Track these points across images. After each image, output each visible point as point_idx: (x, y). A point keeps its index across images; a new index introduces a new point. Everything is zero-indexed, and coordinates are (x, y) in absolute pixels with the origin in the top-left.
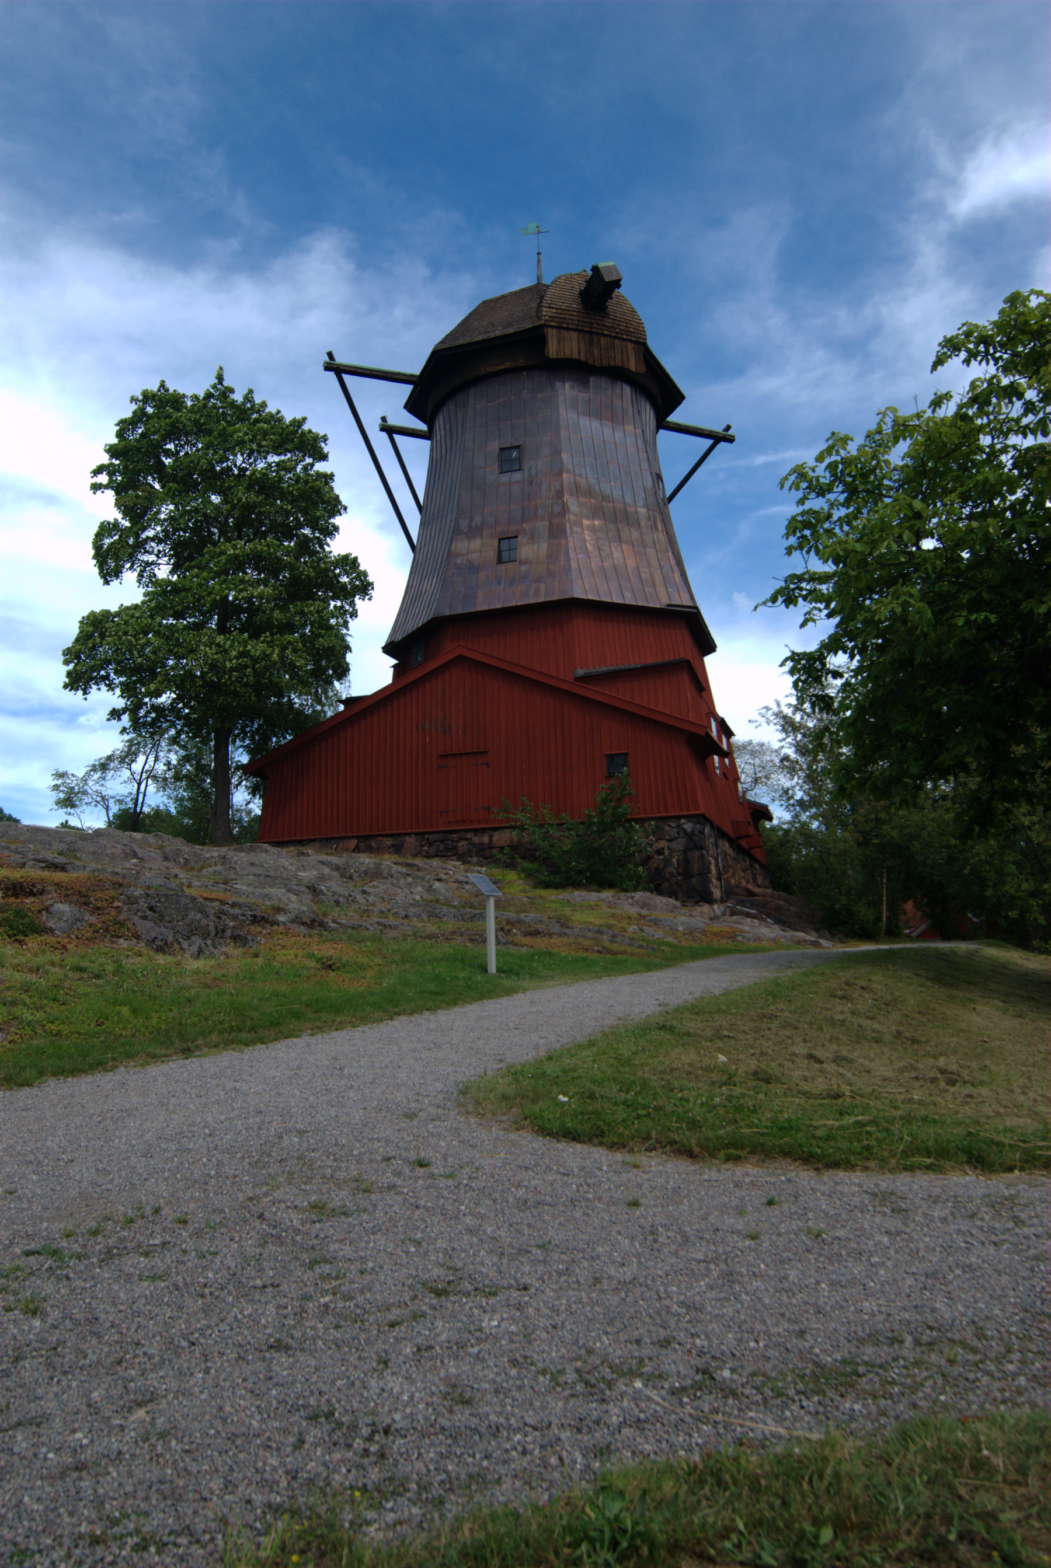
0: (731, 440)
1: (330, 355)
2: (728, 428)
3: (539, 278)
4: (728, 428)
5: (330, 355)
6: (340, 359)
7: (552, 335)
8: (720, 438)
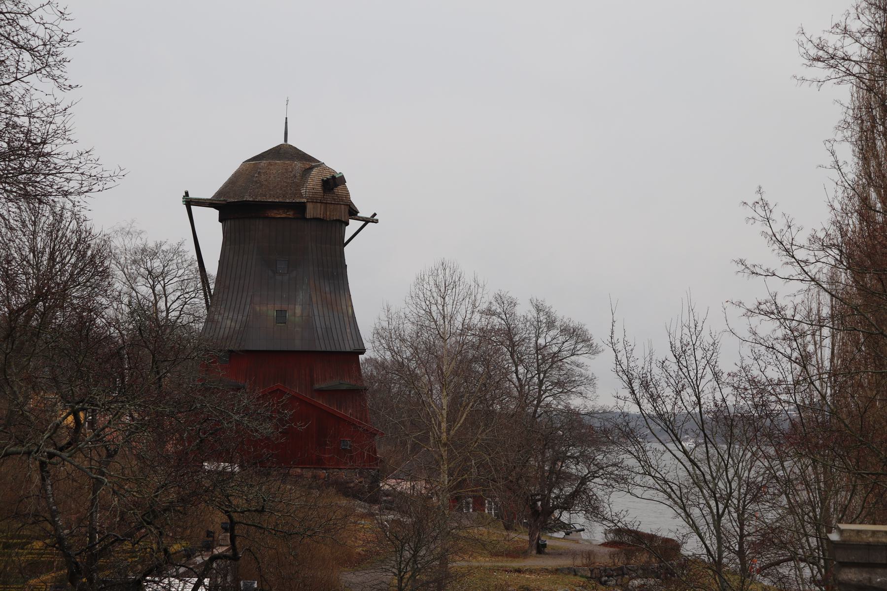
0: (376, 221)
1: (187, 193)
2: (375, 215)
3: (286, 140)
4: (375, 215)
5: (187, 193)
6: (192, 195)
7: (309, 206)
8: (367, 221)
